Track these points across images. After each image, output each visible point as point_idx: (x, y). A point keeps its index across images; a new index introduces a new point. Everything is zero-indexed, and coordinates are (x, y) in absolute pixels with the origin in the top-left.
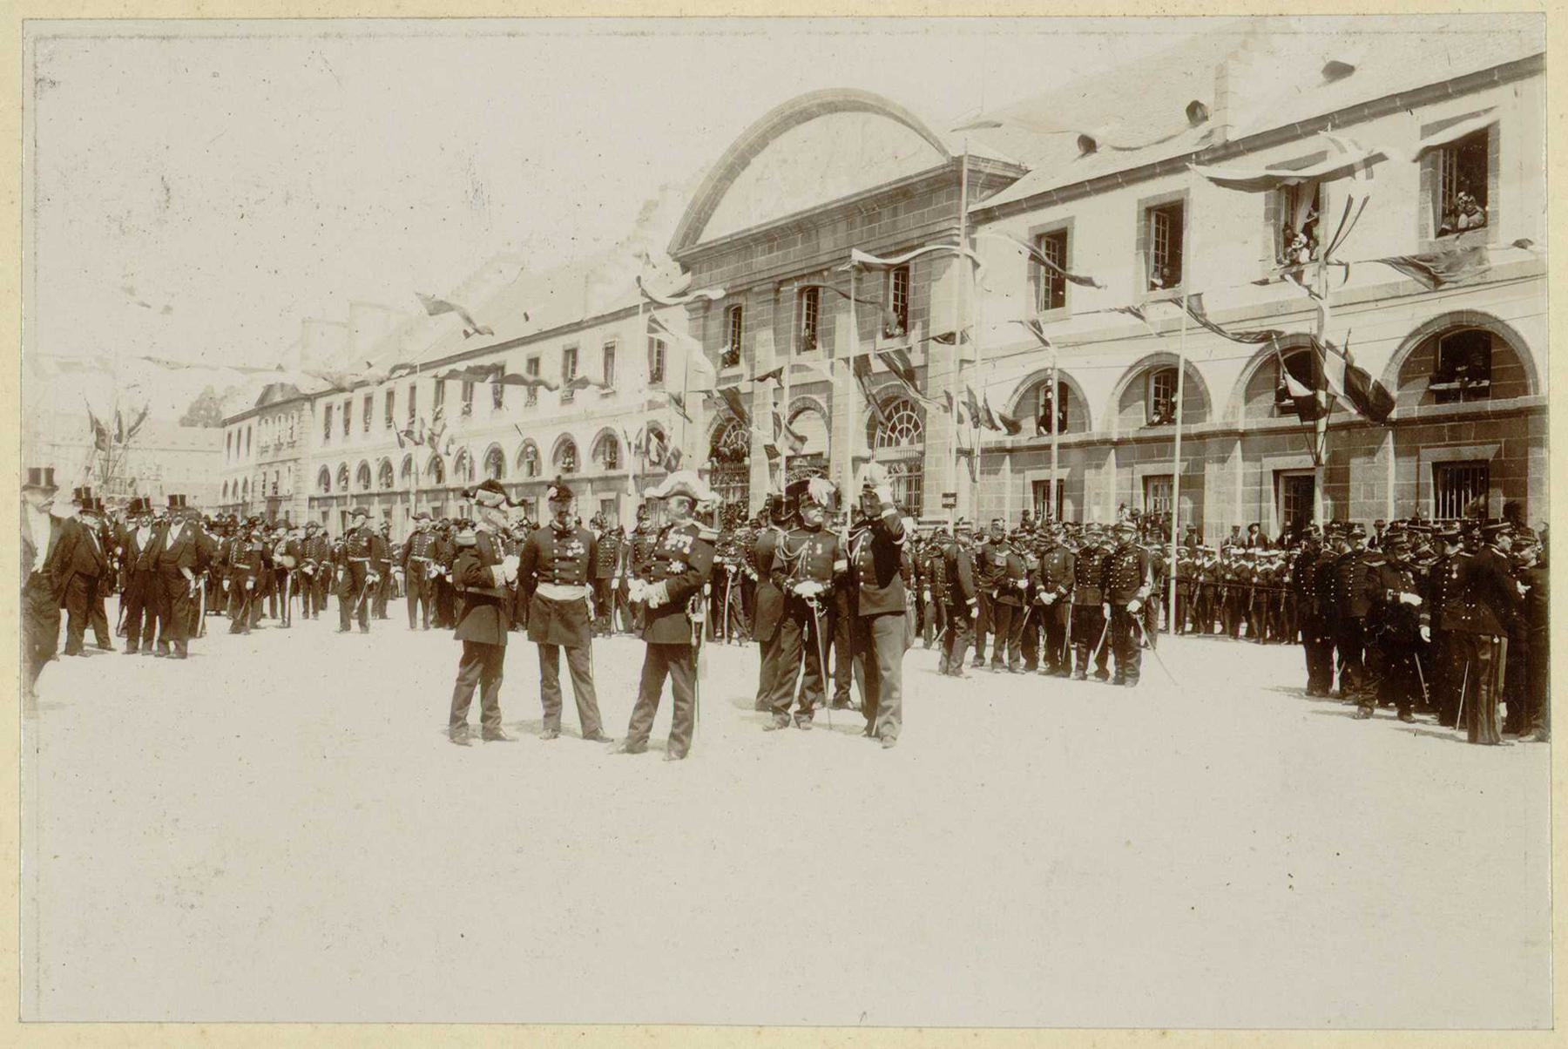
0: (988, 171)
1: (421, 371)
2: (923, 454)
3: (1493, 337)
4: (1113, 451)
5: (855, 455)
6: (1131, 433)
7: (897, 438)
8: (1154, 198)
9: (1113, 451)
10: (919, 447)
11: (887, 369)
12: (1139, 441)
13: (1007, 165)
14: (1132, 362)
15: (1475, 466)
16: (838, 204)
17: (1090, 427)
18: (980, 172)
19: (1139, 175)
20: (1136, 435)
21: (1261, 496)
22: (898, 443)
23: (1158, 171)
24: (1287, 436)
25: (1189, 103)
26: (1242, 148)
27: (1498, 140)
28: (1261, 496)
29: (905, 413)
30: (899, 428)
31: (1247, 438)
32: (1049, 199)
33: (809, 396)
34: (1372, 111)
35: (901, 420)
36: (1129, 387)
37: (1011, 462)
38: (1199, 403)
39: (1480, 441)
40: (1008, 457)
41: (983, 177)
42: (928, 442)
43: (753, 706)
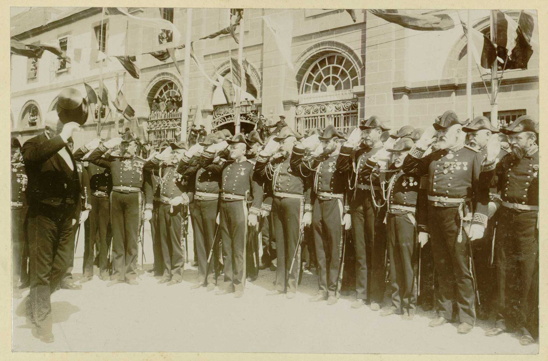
29: (331, 66)
30: (325, 78)
35: (327, 71)
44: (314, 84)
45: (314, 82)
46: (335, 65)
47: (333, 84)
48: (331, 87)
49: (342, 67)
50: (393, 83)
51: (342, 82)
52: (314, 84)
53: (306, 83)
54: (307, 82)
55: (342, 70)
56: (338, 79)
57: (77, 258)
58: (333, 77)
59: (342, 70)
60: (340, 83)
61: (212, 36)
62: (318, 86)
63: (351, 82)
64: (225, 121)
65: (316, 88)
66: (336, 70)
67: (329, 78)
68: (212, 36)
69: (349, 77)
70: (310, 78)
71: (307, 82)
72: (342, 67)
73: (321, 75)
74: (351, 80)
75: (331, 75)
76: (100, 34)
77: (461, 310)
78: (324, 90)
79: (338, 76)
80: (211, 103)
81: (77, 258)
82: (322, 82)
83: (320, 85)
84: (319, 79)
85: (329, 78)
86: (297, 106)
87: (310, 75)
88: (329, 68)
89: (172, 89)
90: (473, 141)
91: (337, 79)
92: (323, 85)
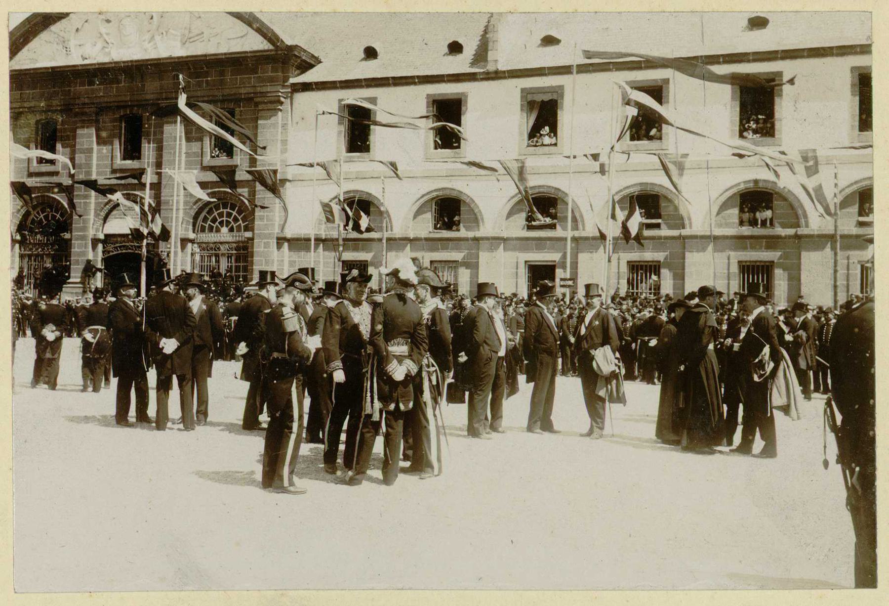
0: (304, 58)
1: (578, 72)
2: (252, 239)
3: (462, 203)
4: (409, 244)
5: (183, 237)
6: (423, 234)
7: (217, 226)
8: (439, 95)
9: (409, 244)
10: (248, 234)
11: (219, 180)
12: (426, 239)
13: (313, 56)
14: (729, 185)
15: (354, 263)
16: (261, 54)
17: (691, 224)
18: (300, 57)
19: (408, 81)
20: (427, 236)
21: (517, 275)
22: (218, 231)
23: (751, 58)
24: (534, 242)
25: (460, 42)
26: (417, 80)
27: (668, 96)
28: (517, 275)
29: (225, 210)
30: (219, 220)
31: (326, 242)
32: (360, 84)
33: (47, 194)
34: (594, 68)
35: (221, 215)
36: (421, 207)
37: (411, 247)
38: (475, 220)
39: (656, 249)
40: (321, 245)
41: (299, 61)
42: (256, 232)
43: (526, 430)
44: (209, 224)
45: (209, 222)
46: (228, 210)
47: (227, 226)
48: (224, 230)
49: (234, 213)
50: (277, 233)
51: (234, 226)
52: (209, 224)
53: (201, 223)
54: (203, 222)
55: (235, 215)
56: (239, 221)
57: (242, 398)
58: (226, 220)
59: (235, 215)
60: (232, 226)
61: (729, 146)
62: (213, 227)
63: (235, 228)
64: (118, 251)
65: (211, 229)
66: (229, 215)
67: (223, 220)
68: (729, 146)
69: (241, 222)
70: (205, 220)
71: (203, 222)
72: (234, 213)
73: (216, 218)
74: (242, 225)
75: (225, 219)
76: (211, 141)
77: (595, 428)
78: (218, 231)
79: (231, 220)
80: (102, 232)
81: (242, 398)
82: (217, 223)
83: (215, 226)
84: (214, 221)
85: (223, 220)
86: (192, 243)
87: (205, 215)
88: (223, 212)
89: (52, 211)
90: (260, 302)
91: (238, 220)
92: (217, 226)
